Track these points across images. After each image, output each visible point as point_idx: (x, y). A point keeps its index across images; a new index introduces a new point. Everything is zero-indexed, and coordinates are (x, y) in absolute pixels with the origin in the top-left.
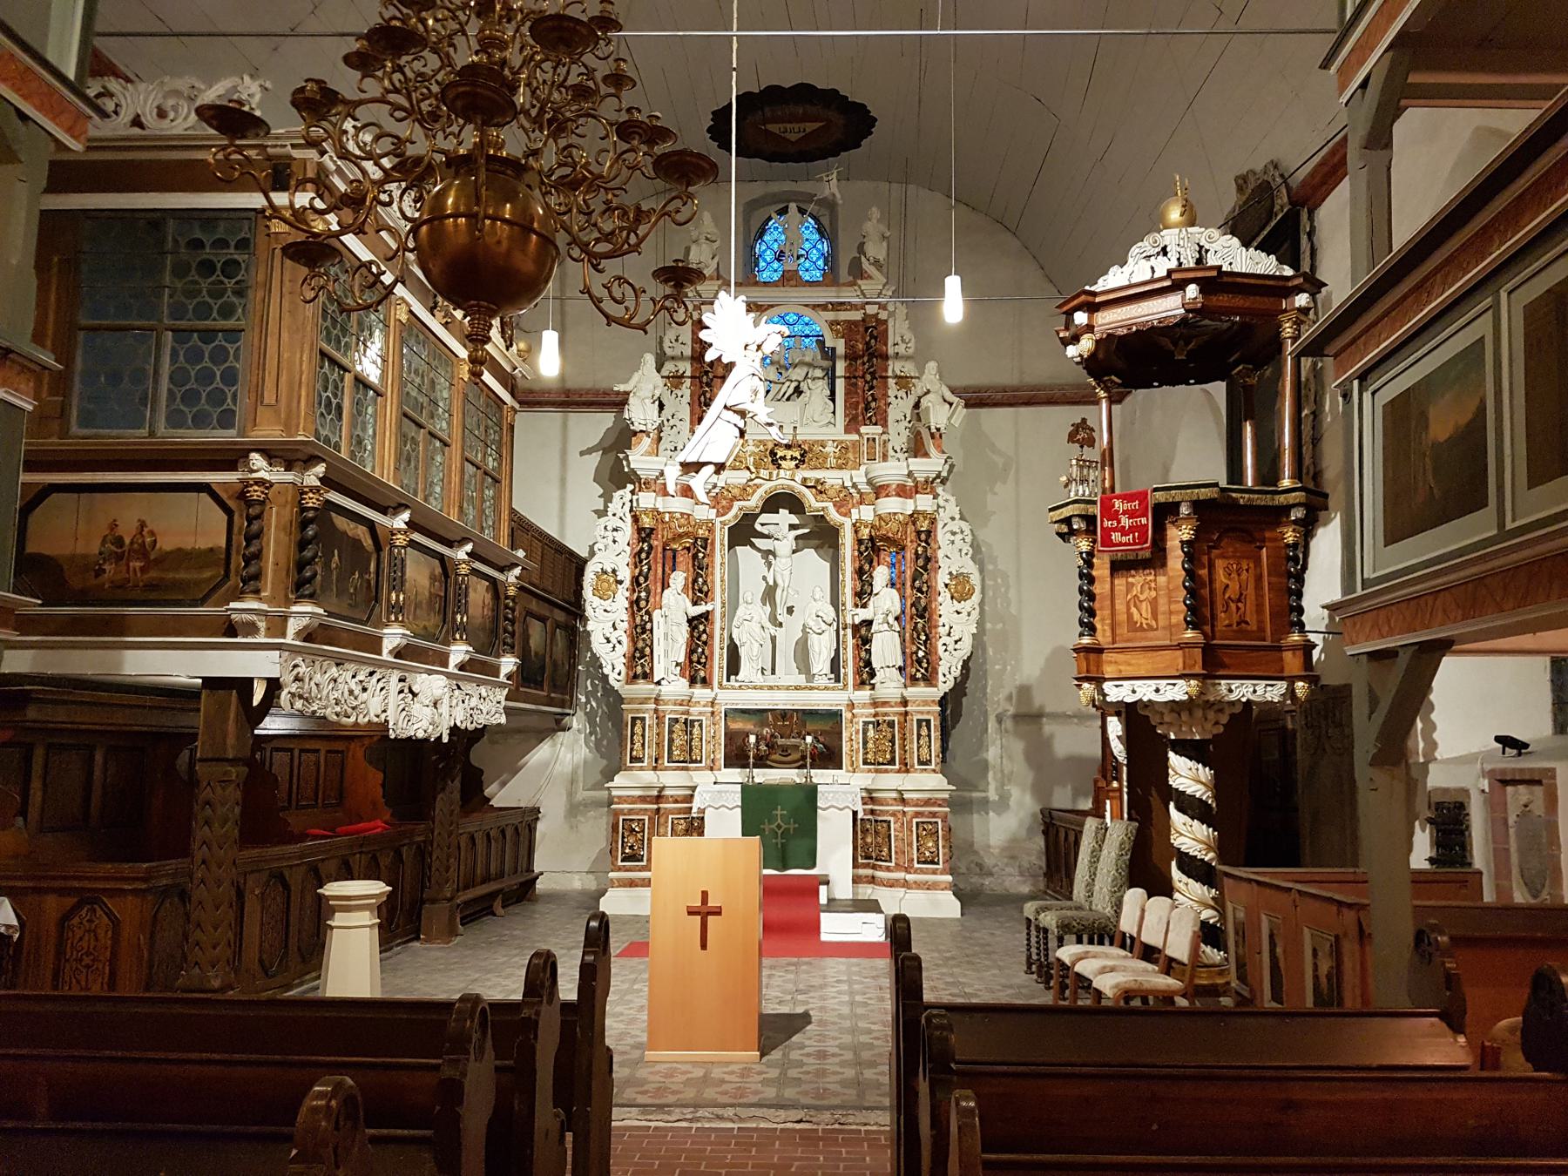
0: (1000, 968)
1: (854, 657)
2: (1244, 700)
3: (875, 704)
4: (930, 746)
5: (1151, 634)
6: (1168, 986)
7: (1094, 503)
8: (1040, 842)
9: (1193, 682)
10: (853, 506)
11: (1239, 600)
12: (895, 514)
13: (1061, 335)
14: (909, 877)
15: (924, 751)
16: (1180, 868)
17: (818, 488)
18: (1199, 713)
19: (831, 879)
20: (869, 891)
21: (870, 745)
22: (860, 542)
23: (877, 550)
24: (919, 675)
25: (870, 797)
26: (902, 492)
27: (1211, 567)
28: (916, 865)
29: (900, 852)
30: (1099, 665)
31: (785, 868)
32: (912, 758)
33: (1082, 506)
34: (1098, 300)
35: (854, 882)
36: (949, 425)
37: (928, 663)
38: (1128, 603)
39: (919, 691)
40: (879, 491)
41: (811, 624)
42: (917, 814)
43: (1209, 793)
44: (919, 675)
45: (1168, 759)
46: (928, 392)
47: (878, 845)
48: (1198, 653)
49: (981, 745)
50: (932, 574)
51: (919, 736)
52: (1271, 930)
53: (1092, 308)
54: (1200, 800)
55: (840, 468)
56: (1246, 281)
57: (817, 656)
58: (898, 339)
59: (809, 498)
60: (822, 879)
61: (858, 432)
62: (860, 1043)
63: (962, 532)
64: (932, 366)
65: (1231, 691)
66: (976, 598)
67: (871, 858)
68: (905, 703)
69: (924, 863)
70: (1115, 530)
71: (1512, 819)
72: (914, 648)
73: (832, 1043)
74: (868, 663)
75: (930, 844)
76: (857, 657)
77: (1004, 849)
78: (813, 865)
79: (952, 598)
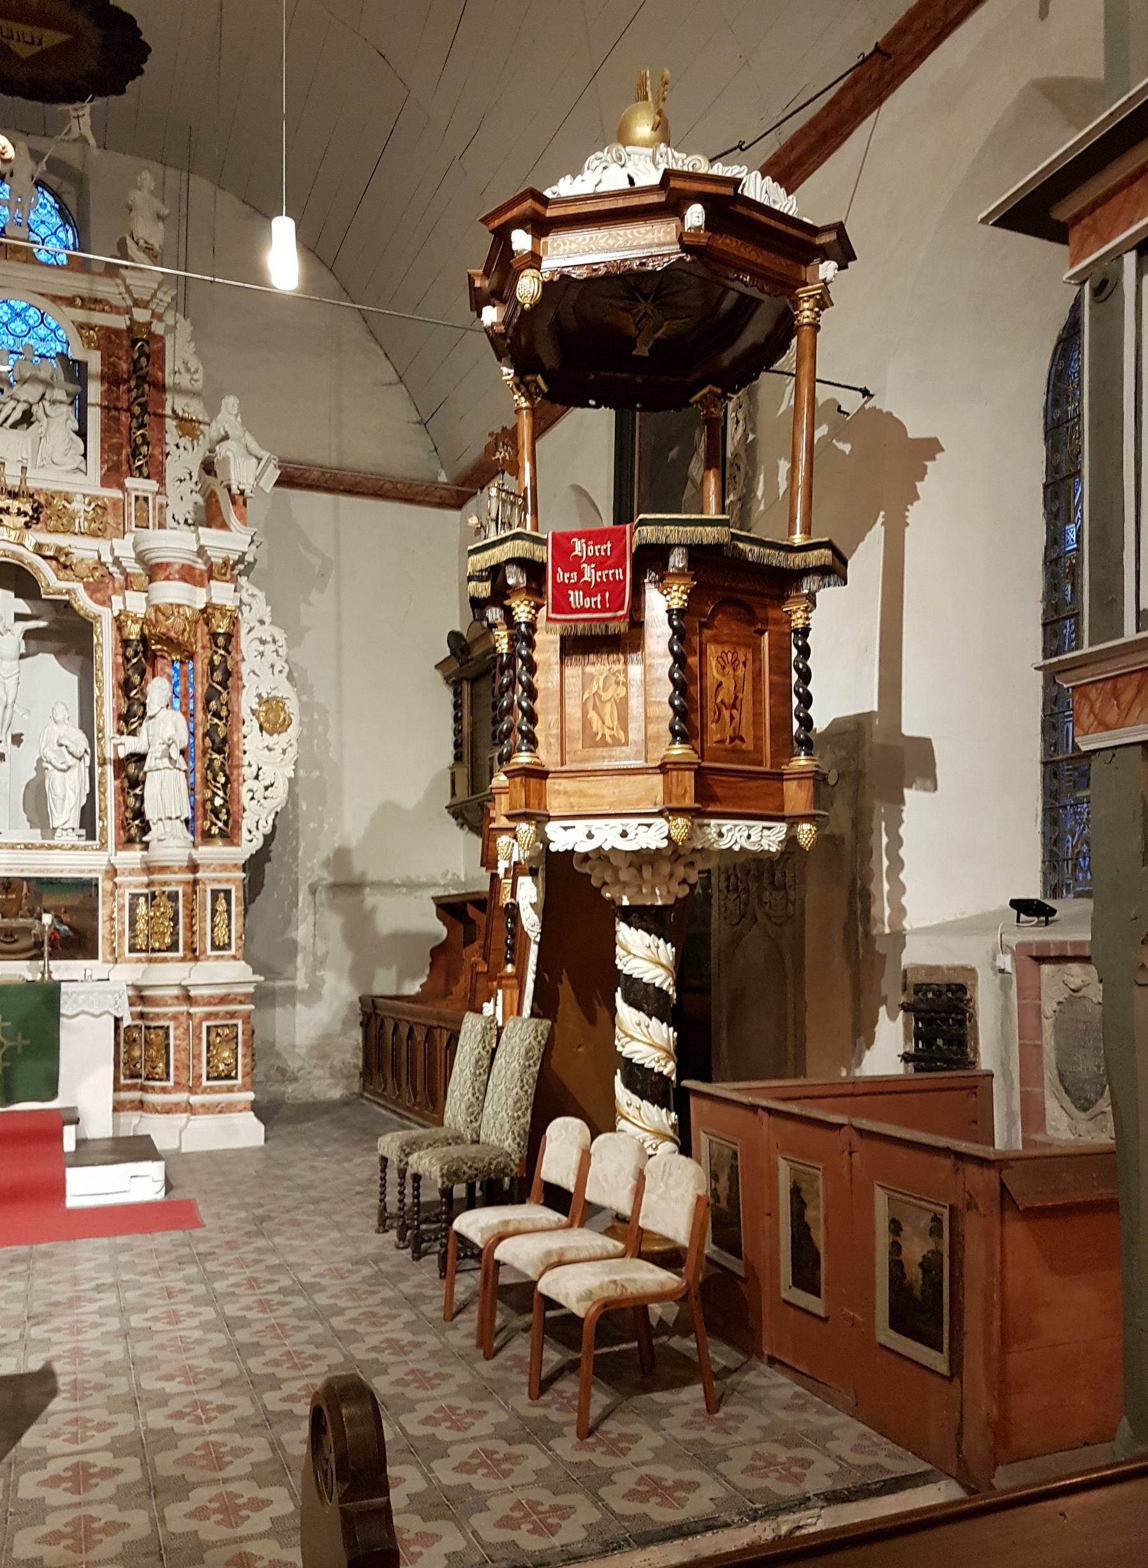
0: (339, 1227)
1: (117, 806)
2: (736, 848)
3: (148, 869)
4: (229, 925)
5: (617, 751)
6: (662, 1284)
7: (543, 542)
8: (357, 1035)
9: (681, 821)
10: (115, 592)
11: (734, 706)
12: (179, 606)
13: (478, 284)
14: (195, 1099)
15: (221, 933)
16: (628, 1085)
17: (61, 561)
18: (666, 868)
19: (82, 1113)
20: (135, 1121)
21: (141, 925)
22: (126, 643)
23: (152, 658)
24: (215, 830)
25: (139, 996)
26: (188, 575)
27: (702, 654)
28: (205, 1083)
29: (183, 1067)
30: (541, 797)
31: (10, 1101)
32: (203, 941)
33: (528, 544)
34: (549, 213)
35: (115, 1110)
36: (257, 488)
37: (228, 813)
38: (584, 704)
39: (214, 852)
40: (154, 571)
41: (51, 756)
42: (209, 1016)
43: (670, 980)
44: (215, 830)
45: (615, 933)
46: (226, 437)
47: (149, 1059)
48: (689, 778)
49: (288, 921)
50: (234, 695)
51: (214, 912)
52: (795, 1183)
53: (541, 227)
54: (660, 989)
55: (94, 535)
56: (763, 219)
57: (59, 803)
58: (179, 365)
59: (47, 573)
60: (66, 1116)
61: (121, 486)
62: (150, 1431)
63: (274, 641)
64: (230, 403)
65: (721, 835)
66: (293, 731)
67: (139, 1076)
68: (194, 867)
69: (216, 1078)
70: (574, 587)
71: (1049, 1008)
72: (209, 794)
73: (87, 1286)
74: (139, 814)
75: (226, 1054)
76: (122, 805)
77: (313, 1048)
78: (54, 1095)
79: (261, 728)
